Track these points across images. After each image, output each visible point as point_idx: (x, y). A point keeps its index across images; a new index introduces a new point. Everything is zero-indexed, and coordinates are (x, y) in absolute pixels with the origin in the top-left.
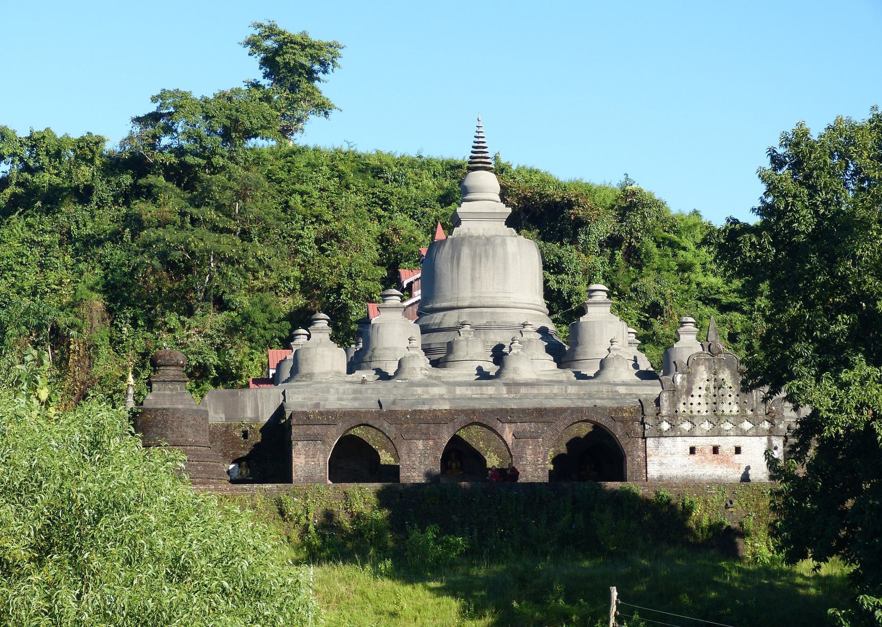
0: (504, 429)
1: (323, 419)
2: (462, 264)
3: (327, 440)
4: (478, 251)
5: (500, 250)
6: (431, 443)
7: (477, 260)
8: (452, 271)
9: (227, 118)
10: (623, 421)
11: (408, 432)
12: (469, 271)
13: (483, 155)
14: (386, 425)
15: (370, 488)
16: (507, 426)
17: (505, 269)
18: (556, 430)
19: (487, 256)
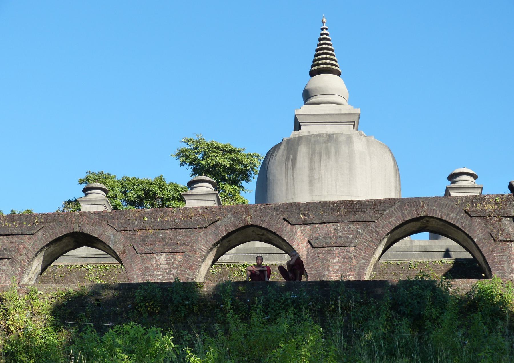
0: (294, 234)
1: (14, 226)
2: (298, 164)
3: (17, 257)
4: (317, 149)
5: (344, 149)
6: (179, 257)
7: (316, 158)
8: (287, 174)
9: (142, 190)
10: (484, 216)
11: (143, 242)
12: (306, 172)
13: (332, 57)
14: (110, 232)
15: (46, 291)
16: (298, 229)
17: (351, 169)
18: (378, 233)
19: (328, 154)
